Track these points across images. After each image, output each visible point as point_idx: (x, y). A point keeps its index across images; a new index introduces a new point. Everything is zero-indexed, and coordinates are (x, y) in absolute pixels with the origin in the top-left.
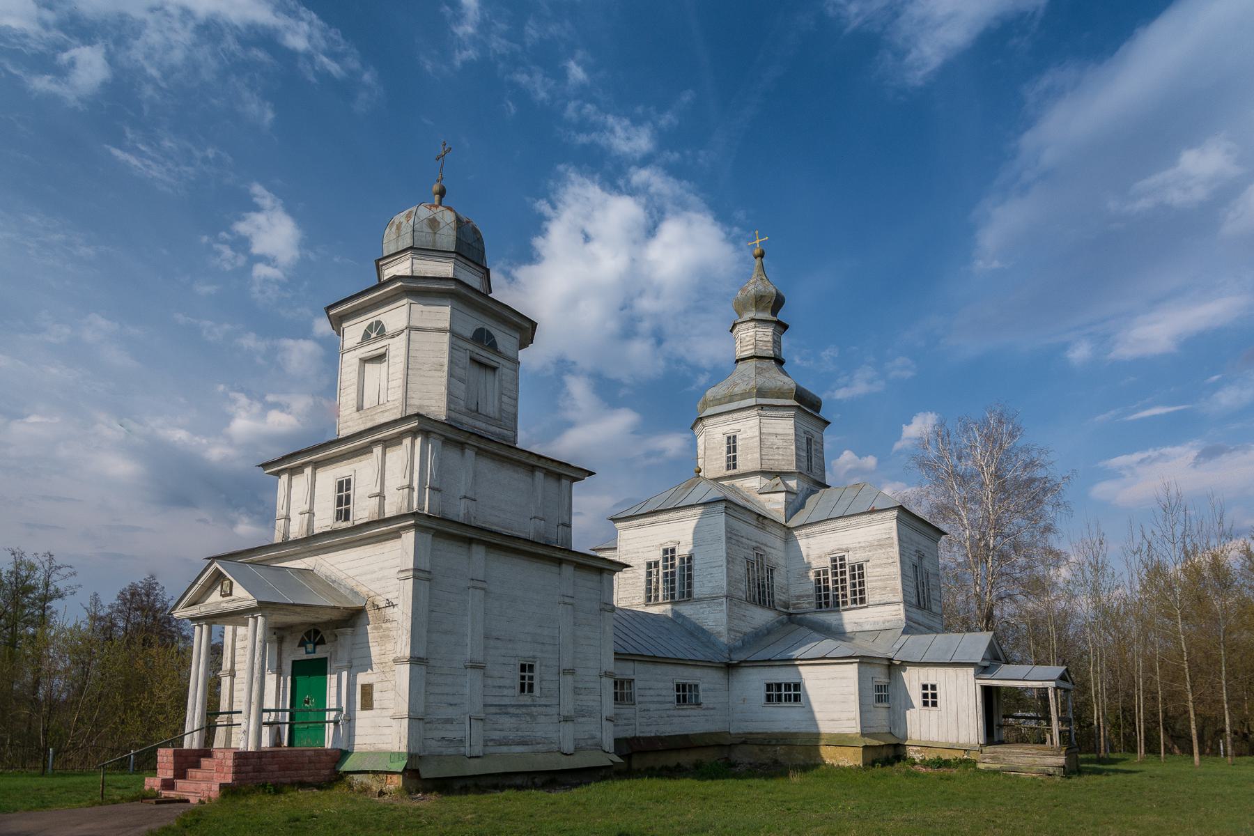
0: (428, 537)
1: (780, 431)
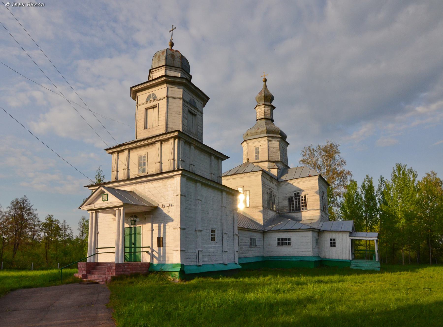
0: (184, 179)
1: (275, 146)
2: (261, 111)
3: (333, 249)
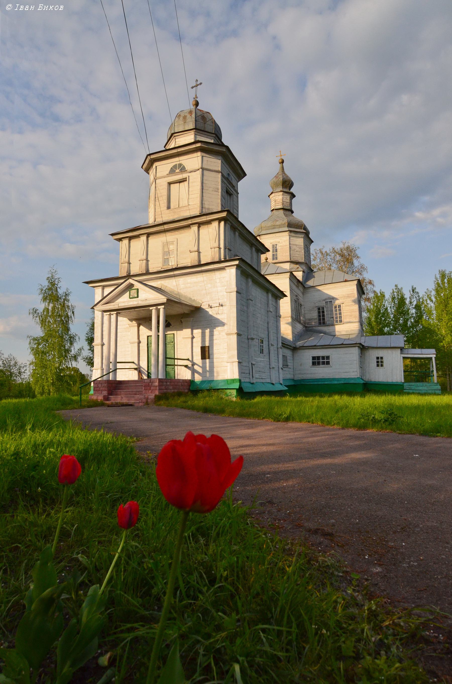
2: (278, 199)
3: (380, 369)
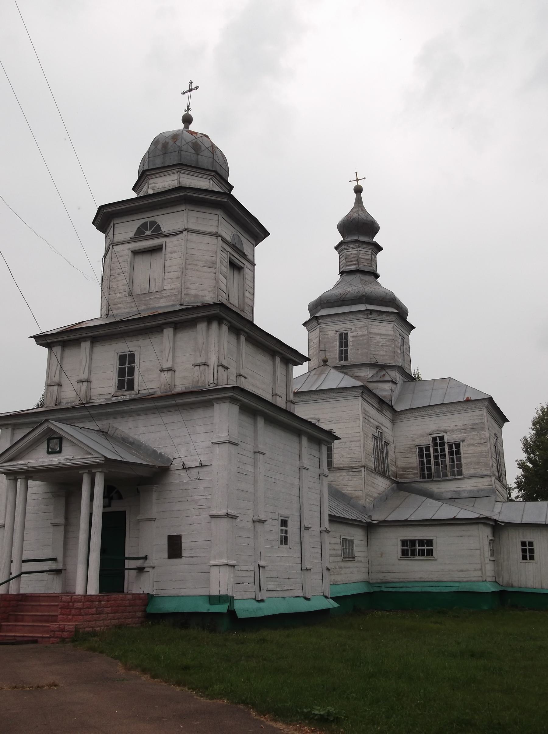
1: (384, 332)
3: (529, 565)
